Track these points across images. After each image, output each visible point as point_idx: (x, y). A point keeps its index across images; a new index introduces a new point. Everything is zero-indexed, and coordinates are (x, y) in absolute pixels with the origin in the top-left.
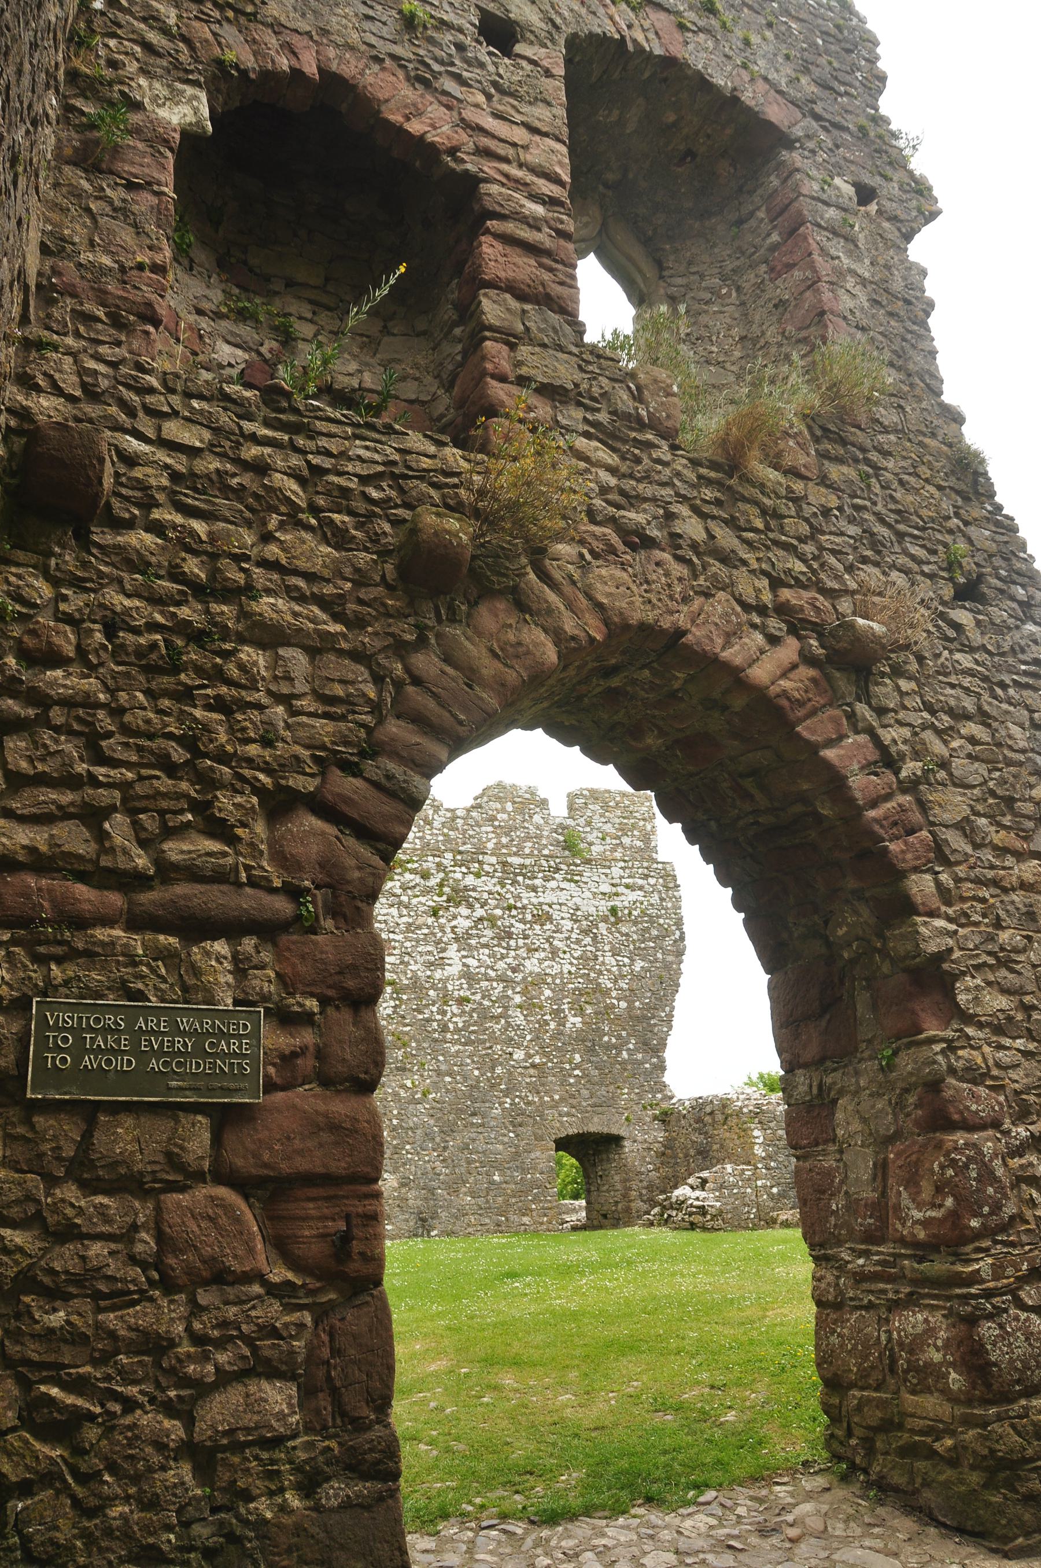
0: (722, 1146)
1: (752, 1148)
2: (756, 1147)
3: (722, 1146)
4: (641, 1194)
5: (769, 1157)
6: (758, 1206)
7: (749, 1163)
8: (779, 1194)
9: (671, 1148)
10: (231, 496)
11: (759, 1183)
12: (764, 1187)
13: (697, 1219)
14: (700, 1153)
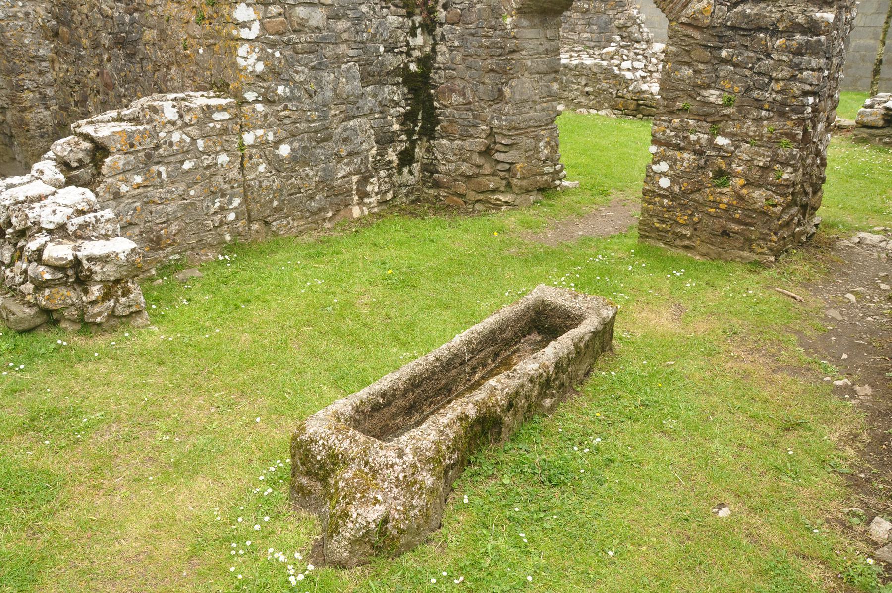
0: (163, 35)
1: (231, 52)
2: (243, 50)
3: (163, 35)
4: (44, 97)
5: (275, 73)
6: (246, 188)
7: (222, 88)
8: (294, 158)
9: (68, 23)
10: (841, 377)
11: (249, 138)
12: (261, 145)
13: (65, 297)
14: (120, 42)
